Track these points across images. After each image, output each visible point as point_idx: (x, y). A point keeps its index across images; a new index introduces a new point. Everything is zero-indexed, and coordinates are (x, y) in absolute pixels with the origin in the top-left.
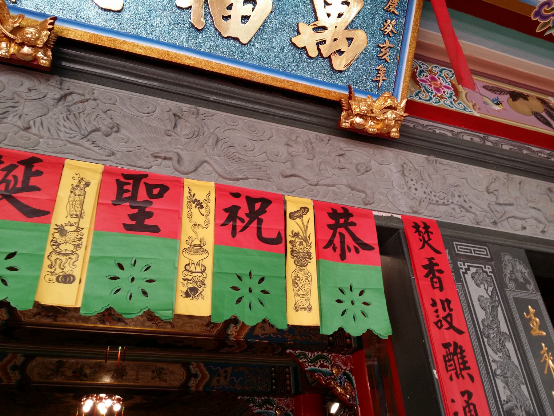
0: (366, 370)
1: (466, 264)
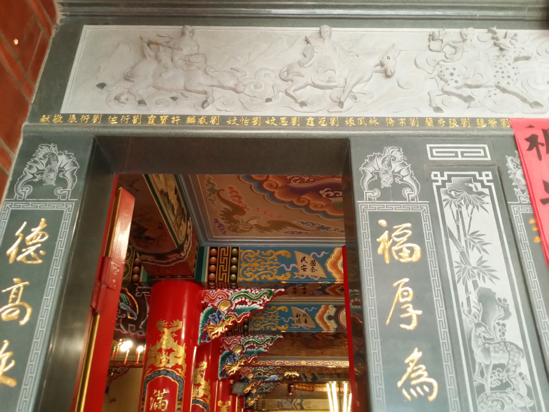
0: (29, 262)
1: (446, 174)
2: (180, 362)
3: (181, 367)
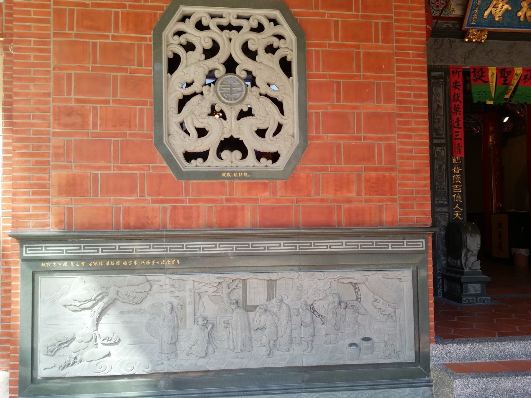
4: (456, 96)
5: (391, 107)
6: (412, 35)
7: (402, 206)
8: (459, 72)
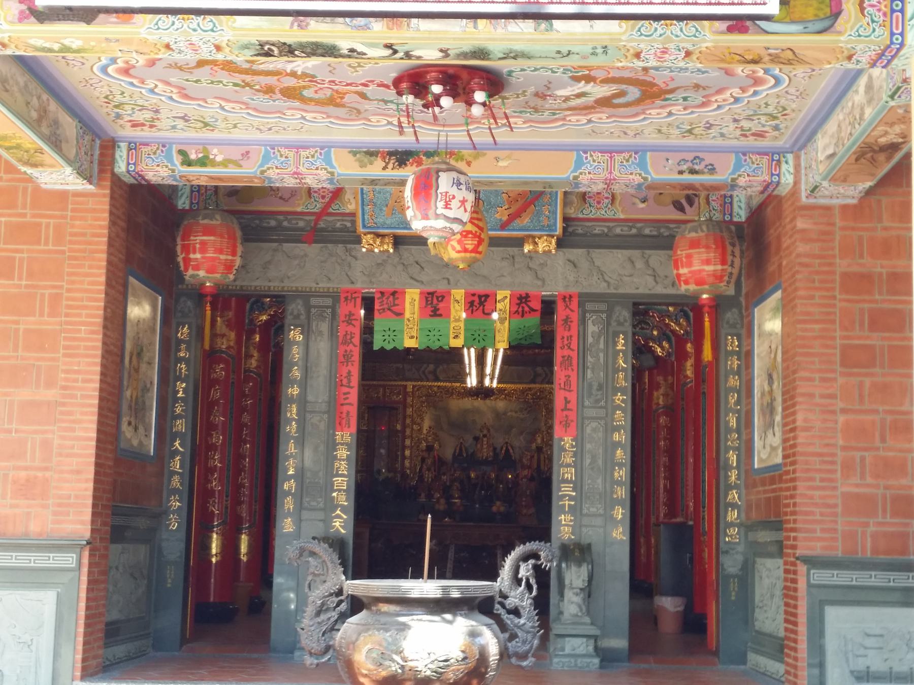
2: (232, 344)
3: (232, 347)
4: (349, 337)
5: (51, 394)
6: (85, 307)
7: (55, 514)
8: (355, 298)
